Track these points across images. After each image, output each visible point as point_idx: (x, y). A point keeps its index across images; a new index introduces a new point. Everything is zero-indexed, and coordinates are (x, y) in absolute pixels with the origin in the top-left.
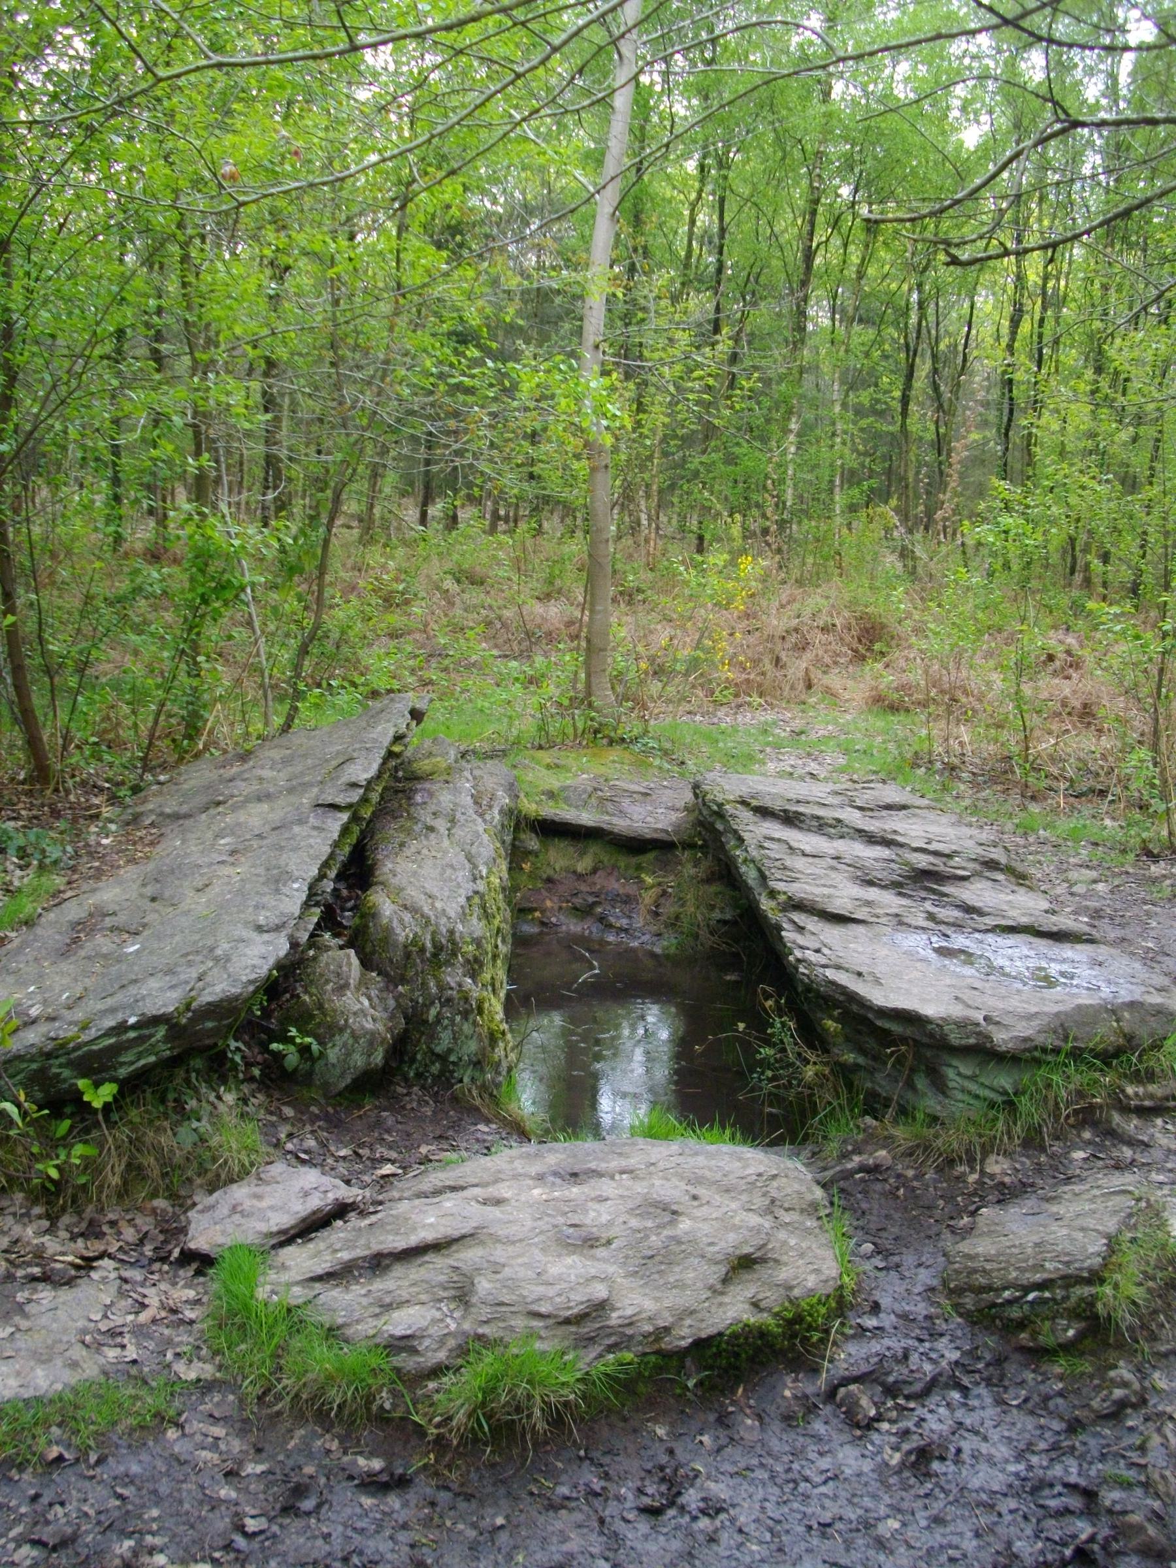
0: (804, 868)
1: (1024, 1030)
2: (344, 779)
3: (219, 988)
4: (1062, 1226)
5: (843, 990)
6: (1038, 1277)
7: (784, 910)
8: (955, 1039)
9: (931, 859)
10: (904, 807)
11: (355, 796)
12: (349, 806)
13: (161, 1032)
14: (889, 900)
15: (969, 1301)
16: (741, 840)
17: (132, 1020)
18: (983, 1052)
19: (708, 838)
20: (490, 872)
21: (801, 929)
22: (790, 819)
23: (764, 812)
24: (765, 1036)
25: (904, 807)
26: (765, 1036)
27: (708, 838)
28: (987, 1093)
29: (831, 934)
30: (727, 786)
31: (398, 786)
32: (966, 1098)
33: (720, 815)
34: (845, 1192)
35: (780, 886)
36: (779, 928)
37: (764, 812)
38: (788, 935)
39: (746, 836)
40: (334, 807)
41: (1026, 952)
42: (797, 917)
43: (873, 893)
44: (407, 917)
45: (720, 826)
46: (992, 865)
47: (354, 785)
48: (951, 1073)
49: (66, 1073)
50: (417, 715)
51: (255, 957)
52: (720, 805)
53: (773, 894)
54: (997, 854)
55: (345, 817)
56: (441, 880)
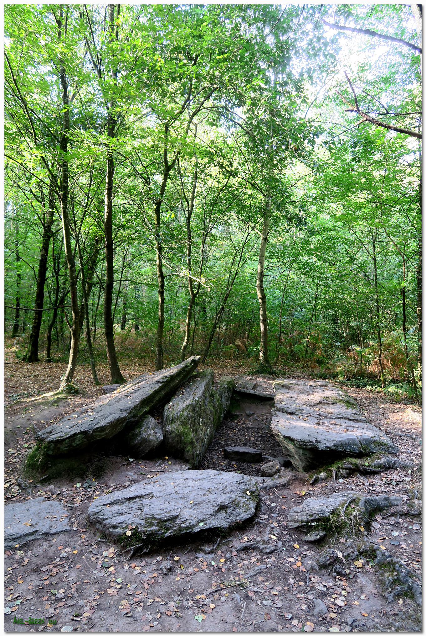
12: (163, 382)
42: (277, 413)
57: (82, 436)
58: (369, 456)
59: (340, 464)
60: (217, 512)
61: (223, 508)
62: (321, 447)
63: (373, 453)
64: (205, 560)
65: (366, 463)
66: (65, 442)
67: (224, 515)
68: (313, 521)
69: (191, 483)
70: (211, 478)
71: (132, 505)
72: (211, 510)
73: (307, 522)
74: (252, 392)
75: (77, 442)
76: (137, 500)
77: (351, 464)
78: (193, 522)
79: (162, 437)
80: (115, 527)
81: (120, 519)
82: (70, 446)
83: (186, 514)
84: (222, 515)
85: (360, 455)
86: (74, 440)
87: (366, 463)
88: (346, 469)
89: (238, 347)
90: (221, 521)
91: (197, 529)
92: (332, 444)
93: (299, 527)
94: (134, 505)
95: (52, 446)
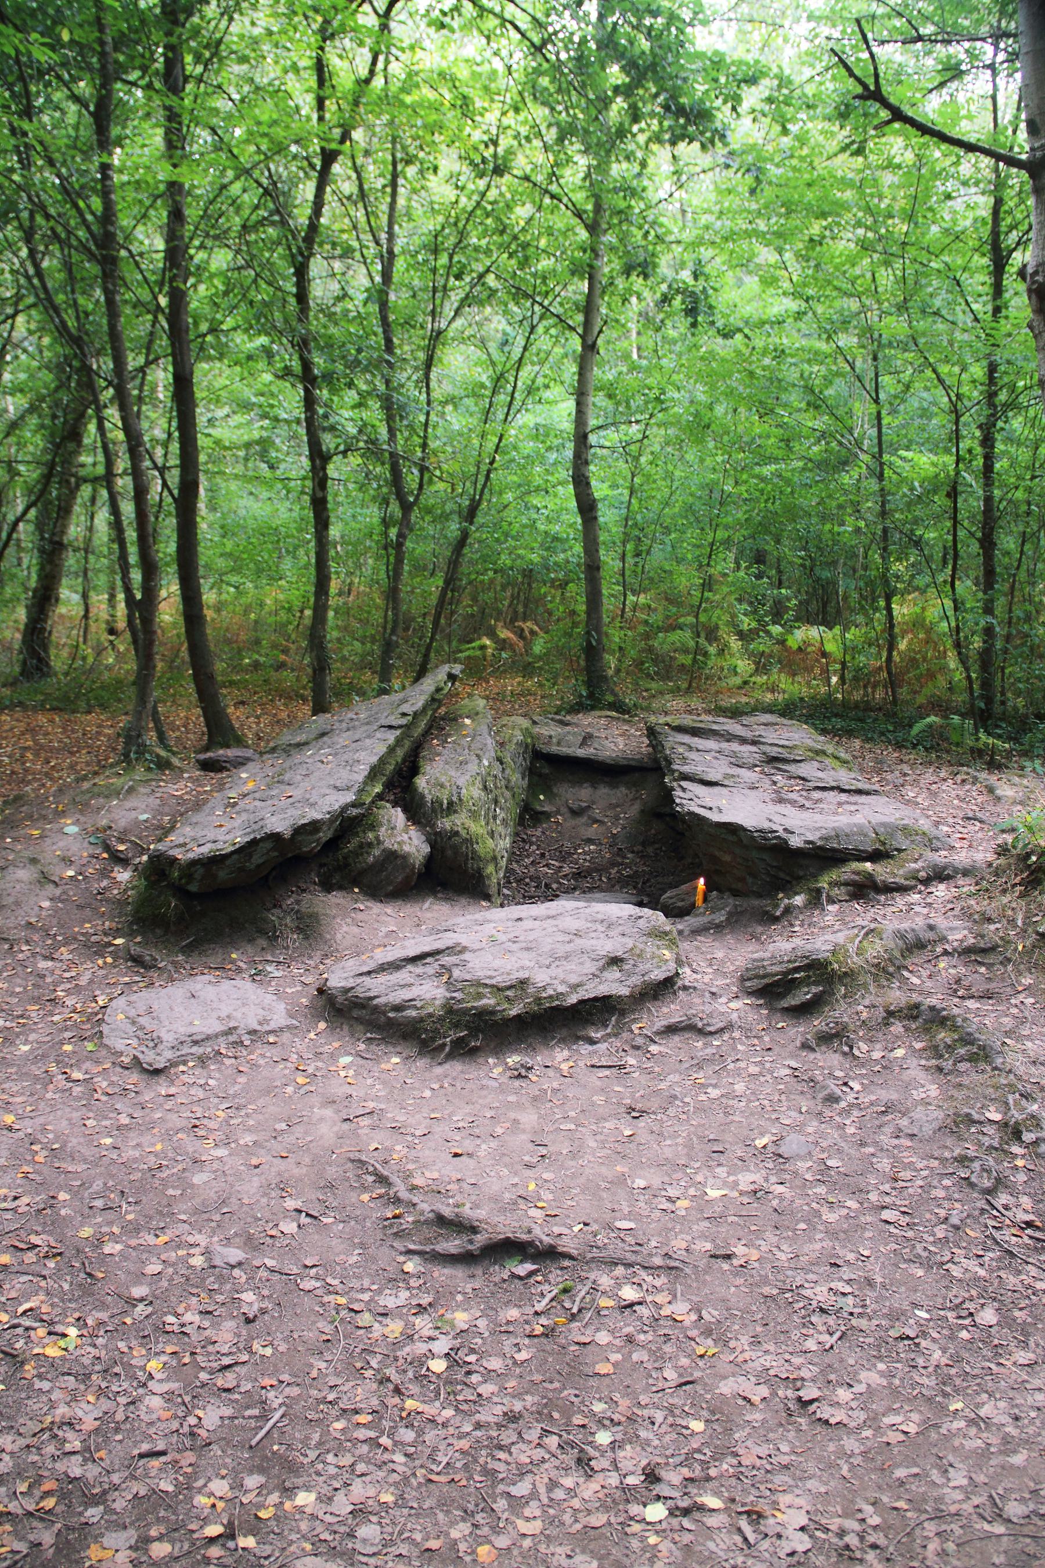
11: (404, 721)
12: (400, 727)
22: (695, 732)
40: (390, 727)
42: (684, 784)
47: (404, 715)
55: (398, 732)
57: (269, 845)
58: (891, 857)
59: (834, 875)
60: (602, 969)
61: (615, 961)
62: (795, 842)
63: (899, 850)
64: (603, 1046)
65: (880, 871)
66: (228, 862)
67: (618, 975)
68: (797, 970)
69: (527, 924)
70: (575, 913)
71: (419, 970)
72: (591, 967)
73: (785, 974)
74: (581, 753)
75: (257, 859)
76: (429, 960)
77: (858, 873)
78: (562, 989)
79: (426, 849)
80: (398, 1008)
81: (405, 995)
82: (241, 870)
83: (541, 978)
84: (614, 974)
85: (876, 856)
86: (251, 856)
87: (880, 871)
88: (846, 884)
89: (503, 645)
90: (614, 985)
91: (573, 999)
92: (818, 834)
93: (767, 985)
94: (431, 967)
95: (200, 871)
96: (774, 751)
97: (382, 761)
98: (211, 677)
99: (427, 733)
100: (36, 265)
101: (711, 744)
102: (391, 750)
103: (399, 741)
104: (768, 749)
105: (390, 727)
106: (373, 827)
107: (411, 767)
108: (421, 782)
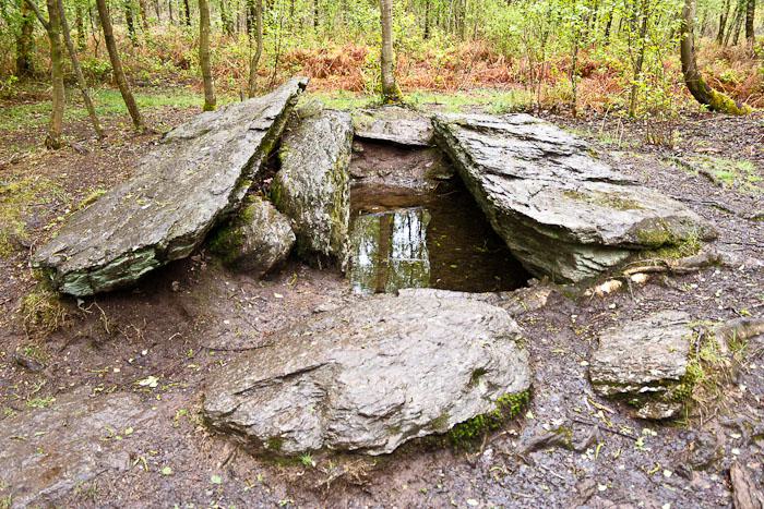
0: (489, 153)
1: (621, 232)
2: (265, 115)
3: (188, 227)
4: (650, 342)
5: (519, 214)
6: (647, 379)
7: (481, 174)
8: (584, 239)
9: (552, 146)
10: (463, 126)
11: (269, 124)
12: (266, 129)
13: (152, 254)
14: (531, 168)
15: (605, 390)
16: (457, 141)
17: (135, 248)
18: (599, 247)
19: (440, 144)
20: (338, 160)
21: (493, 183)
22: (481, 130)
23: (468, 127)
24: (483, 245)
25: (463, 126)
26: (483, 245)
27: (440, 144)
28: (595, 266)
29: (507, 184)
30: (450, 116)
31: (289, 124)
32: (585, 269)
33: (447, 130)
34: (532, 328)
35: (479, 162)
36: (480, 182)
37: (468, 127)
38: (487, 186)
39: (460, 139)
40: (259, 130)
41: (335, 151)
42: (489, 176)
43: (522, 163)
44: (298, 184)
45: (446, 135)
46: (582, 148)
47: (268, 119)
48: (578, 257)
49: (103, 278)
50: (302, 86)
51: (205, 209)
52: (446, 125)
53: (476, 166)
54: (582, 142)
55: (264, 134)
56: (315, 166)
96: (548, 147)
97: (252, 161)
98: (207, 41)
99: (285, 131)
100: (211, 350)
101: (501, 141)
102: (259, 149)
103: (265, 142)
104: (540, 145)
105: (259, 130)
106: (246, 221)
107: (274, 164)
108: (285, 176)
